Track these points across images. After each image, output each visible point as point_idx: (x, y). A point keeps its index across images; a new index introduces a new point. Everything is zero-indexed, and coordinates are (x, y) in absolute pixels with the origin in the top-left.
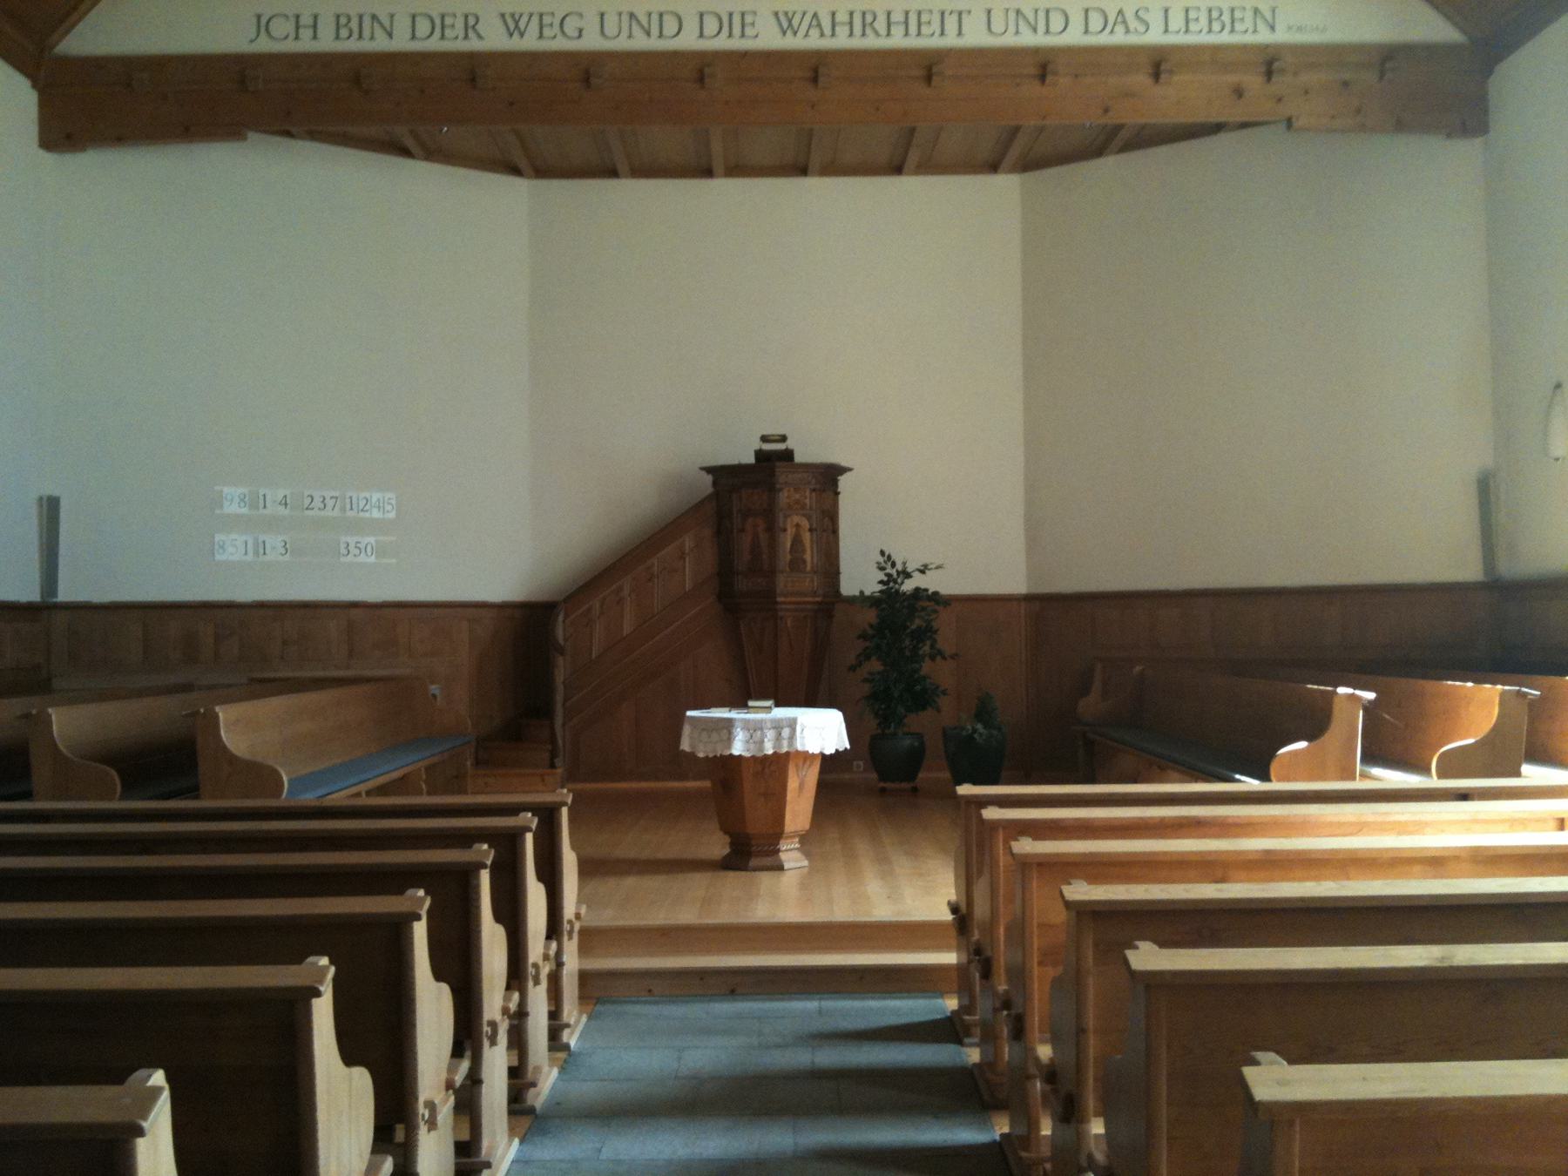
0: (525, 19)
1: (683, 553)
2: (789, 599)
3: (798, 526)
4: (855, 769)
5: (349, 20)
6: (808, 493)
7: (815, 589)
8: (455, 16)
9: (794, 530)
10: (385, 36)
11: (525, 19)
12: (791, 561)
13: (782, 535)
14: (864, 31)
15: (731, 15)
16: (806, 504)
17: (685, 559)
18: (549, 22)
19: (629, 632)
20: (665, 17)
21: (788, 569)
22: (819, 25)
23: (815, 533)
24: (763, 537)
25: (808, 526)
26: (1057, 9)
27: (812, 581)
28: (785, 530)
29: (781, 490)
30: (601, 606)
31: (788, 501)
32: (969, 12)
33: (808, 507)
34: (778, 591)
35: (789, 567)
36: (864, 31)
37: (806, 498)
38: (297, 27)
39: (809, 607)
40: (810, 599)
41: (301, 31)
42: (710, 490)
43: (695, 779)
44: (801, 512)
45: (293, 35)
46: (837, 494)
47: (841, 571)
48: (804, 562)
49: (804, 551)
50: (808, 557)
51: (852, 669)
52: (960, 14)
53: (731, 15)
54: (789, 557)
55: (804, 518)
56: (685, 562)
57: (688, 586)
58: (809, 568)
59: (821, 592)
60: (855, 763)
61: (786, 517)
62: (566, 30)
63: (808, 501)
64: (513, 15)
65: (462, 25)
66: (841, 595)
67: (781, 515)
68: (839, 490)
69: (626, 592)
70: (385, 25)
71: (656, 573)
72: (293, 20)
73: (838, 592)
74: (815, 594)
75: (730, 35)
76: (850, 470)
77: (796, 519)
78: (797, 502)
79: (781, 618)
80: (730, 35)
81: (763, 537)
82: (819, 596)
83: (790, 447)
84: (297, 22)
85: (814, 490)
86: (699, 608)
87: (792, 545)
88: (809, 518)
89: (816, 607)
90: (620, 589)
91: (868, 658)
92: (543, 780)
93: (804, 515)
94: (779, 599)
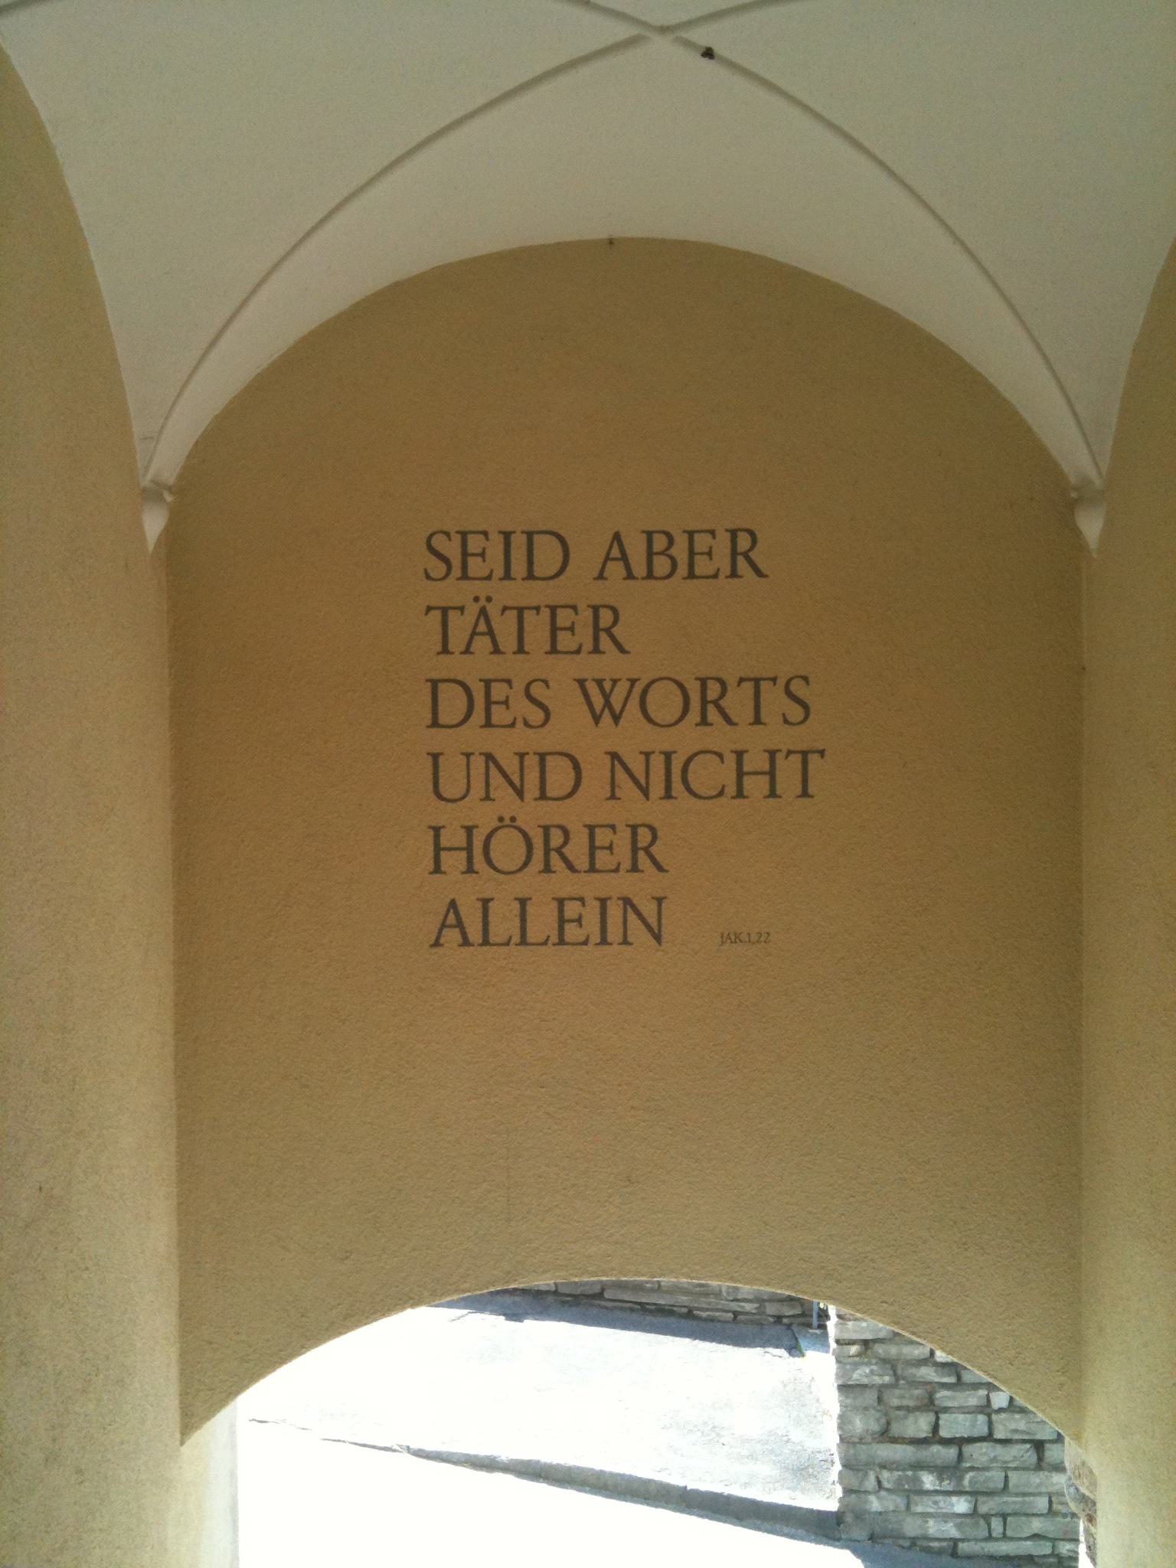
0: (622, 689)
5: (671, 541)
8: (574, 608)
10: (637, 793)
11: (622, 689)
14: (596, 640)
15: (668, 795)
18: (568, 624)
20: (551, 761)
22: (624, 558)
26: (644, 825)
32: (822, 753)
36: (596, 640)
38: (740, 774)
41: (746, 780)
45: (731, 790)
52: (523, 941)
53: (668, 795)
62: (567, 763)
64: (599, 683)
65: (728, 551)
70: (635, 916)
72: (731, 760)
75: (668, 756)
80: (668, 756)
84: (740, 763)
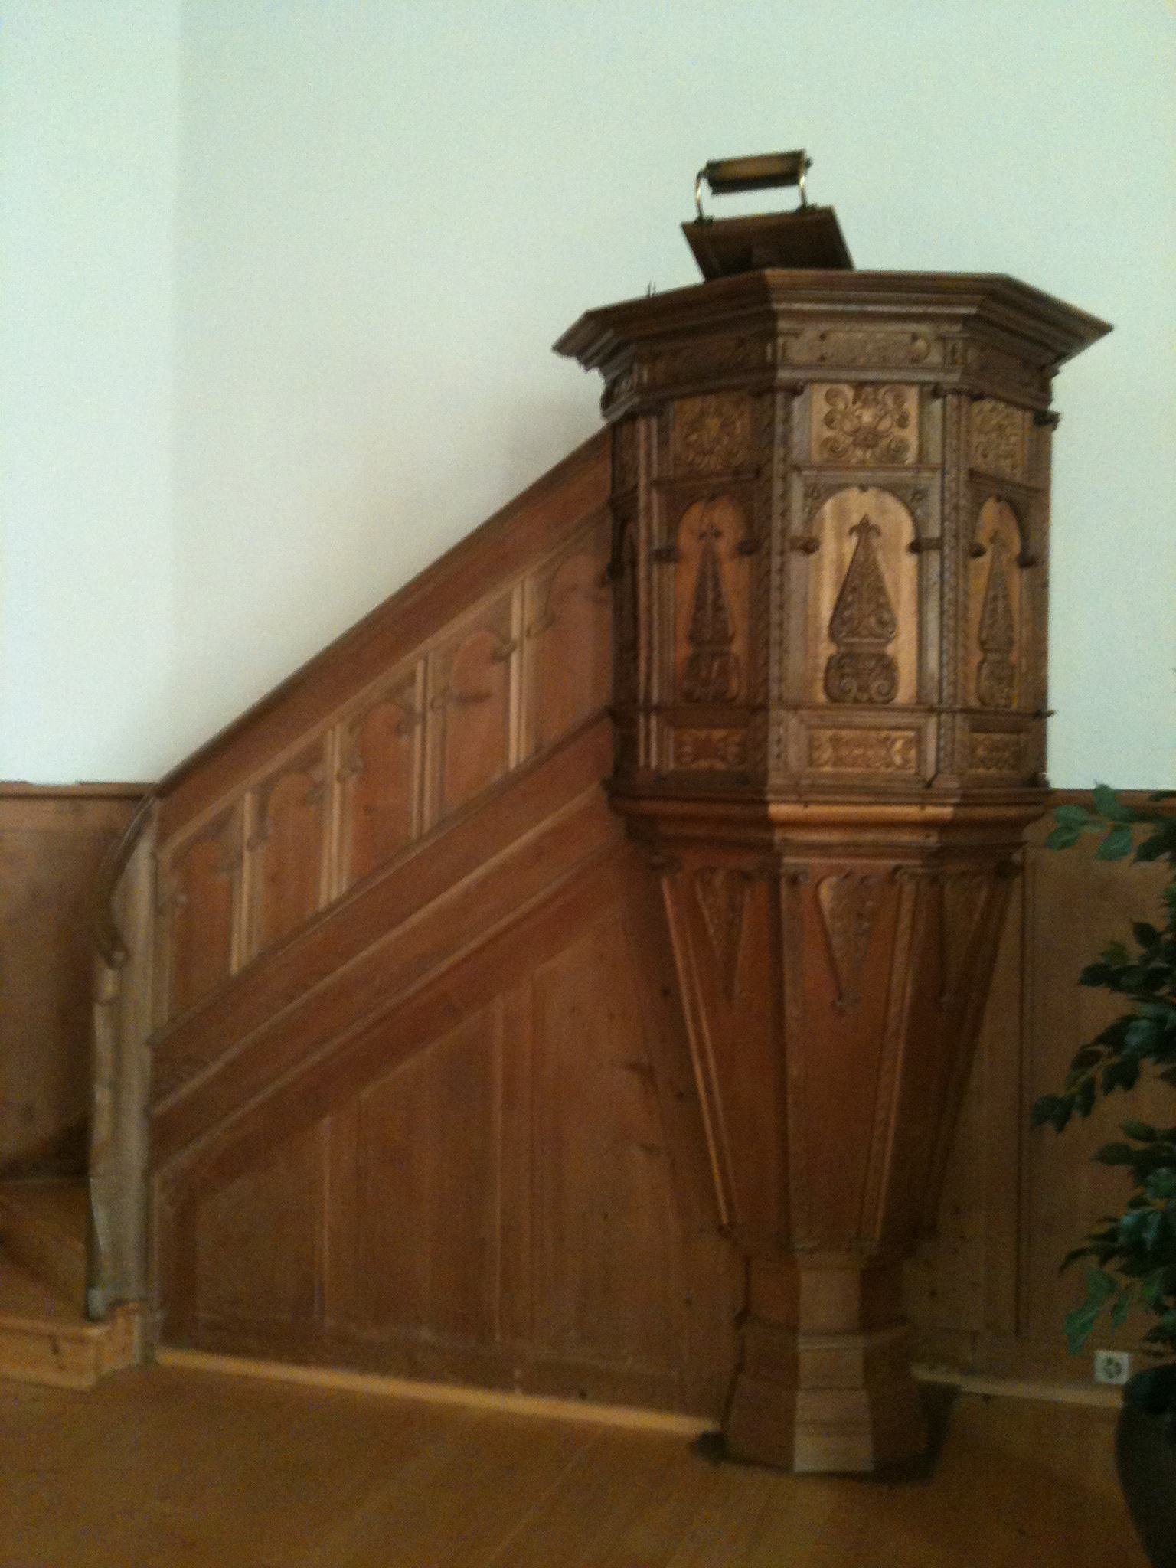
1: (506, 639)
2: (815, 811)
3: (865, 529)
4: (1101, 1377)
6: (911, 405)
7: (930, 771)
9: (851, 544)
12: (835, 666)
13: (797, 562)
16: (902, 447)
17: (506, 658)
19: (334, 895)
21: (821, 698)
23: (934, 558)
24: (734, 575)
25: (907, 536)
27: (919, 741)
28: (810, 546)
29: (795, 390)
30: (262, 811)
31: (828, 433)
33: (911, 457)
34: (775, 780)
35: (827, 689)
37: (903, 422)
39: (904, 837)
40: (912, 812)
42: (595, 422)
43: (532, 1388)
44: (881, 476)
46: (1046, 421)
47: (1054, 700)
48: (888, 667)
49: (887, 626)
50: (903, 648)
51: (1058, 1113)
54: (826, 650)
55: (890, 501)
56: (508, 667)
57: (517, 751)
58: (905, 692)
59: (950, 783)
60: (1102, 1355)
61: (816, 495)
63: (911, 435)
66: (1046, 784)
67: (797, 488)
68: (1053, 407)
69: (334, 761)
71: (418, 707)
73: (1036, 780)
74: (927, 792)
76: (1099, 329)
77: (859, 504)
78: (868, 438)
79: (794, 881)
81: (734, 575)
82: (939, 800)
83: (818, 198)
85: (936, 392)
86: (545, 824)
87: (840, 606)
88: (912, 498)
89: (933, 840)
90: (314, 757)
91: (1125, 1077)
92: (56, 1350)
93: (891, 489)
94: (778, 810)
